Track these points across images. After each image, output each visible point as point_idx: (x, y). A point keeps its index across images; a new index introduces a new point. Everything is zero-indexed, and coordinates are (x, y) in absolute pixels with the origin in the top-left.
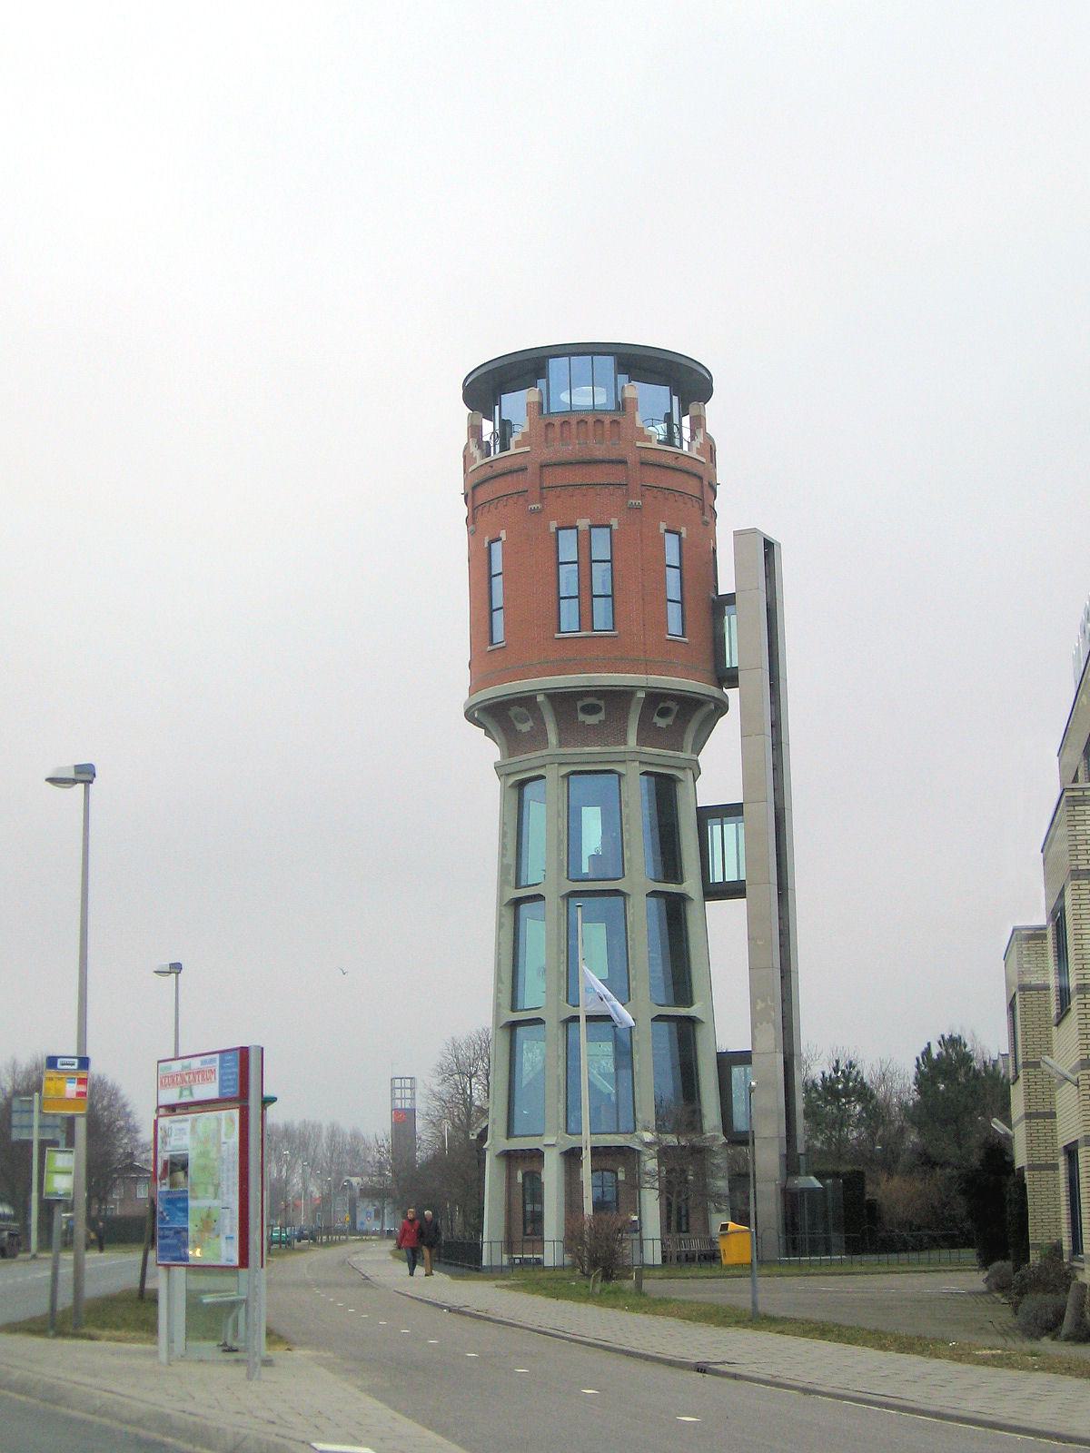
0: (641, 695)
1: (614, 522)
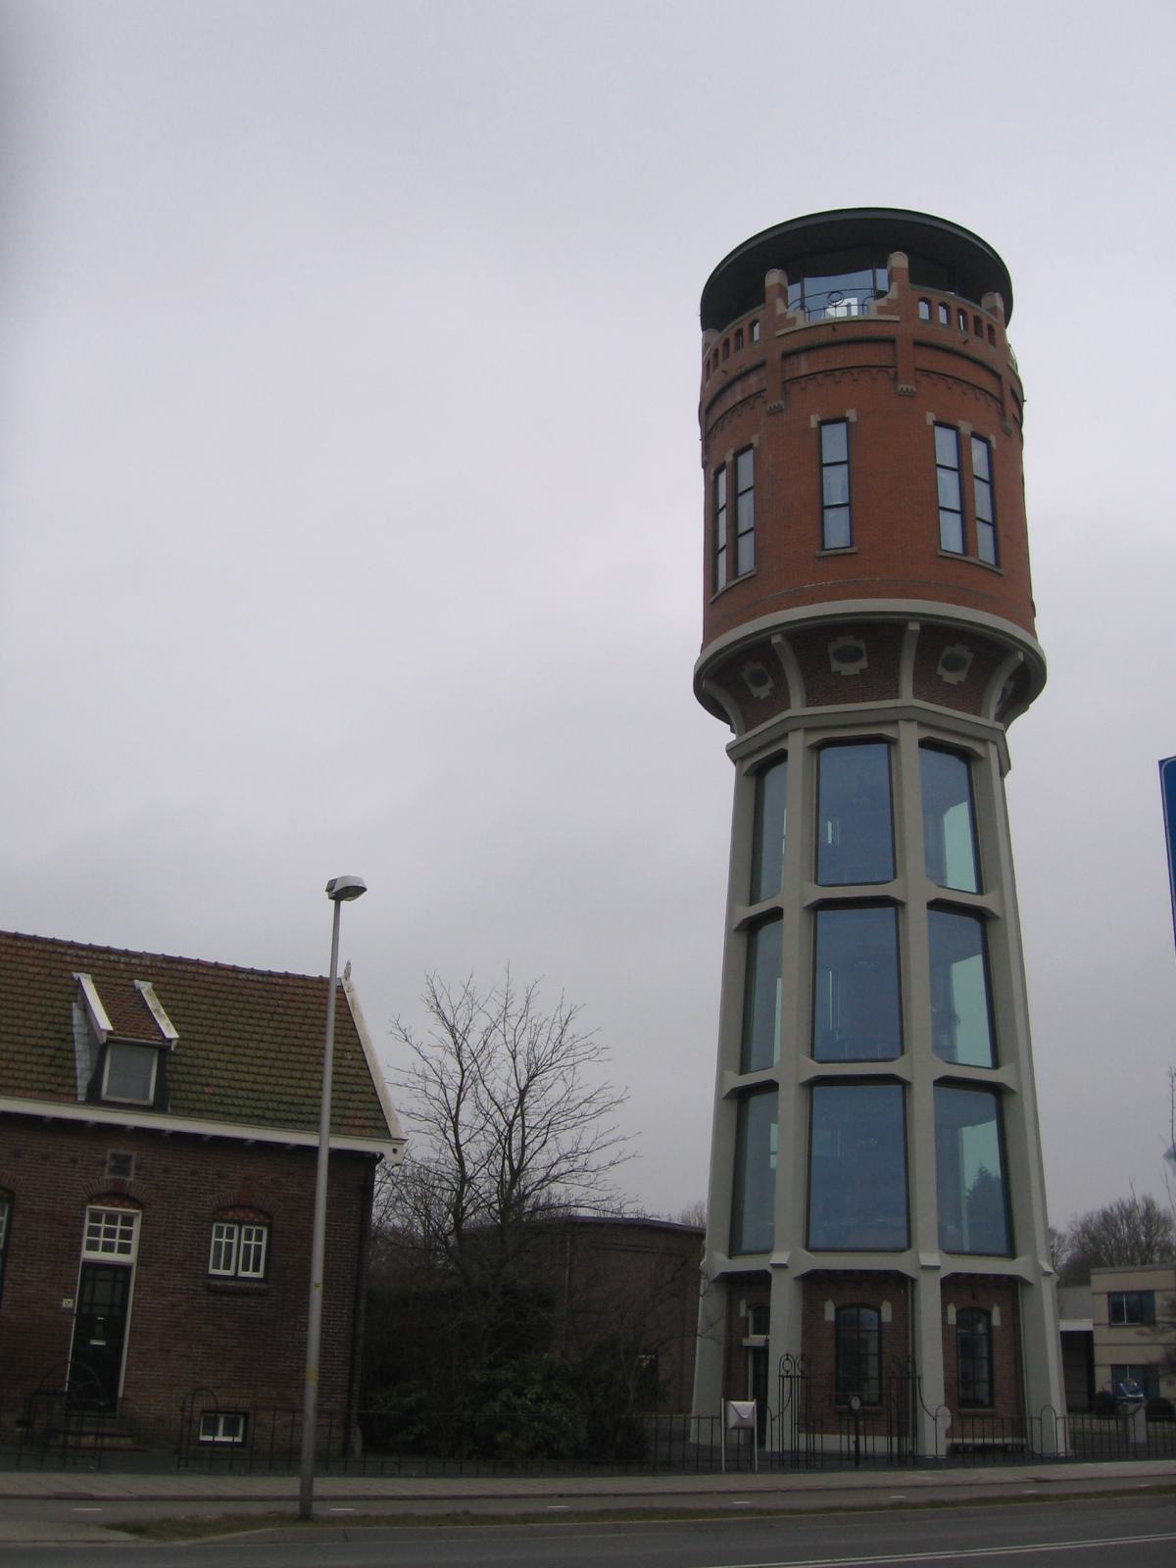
0: (914, 627)
1: (851, 414)
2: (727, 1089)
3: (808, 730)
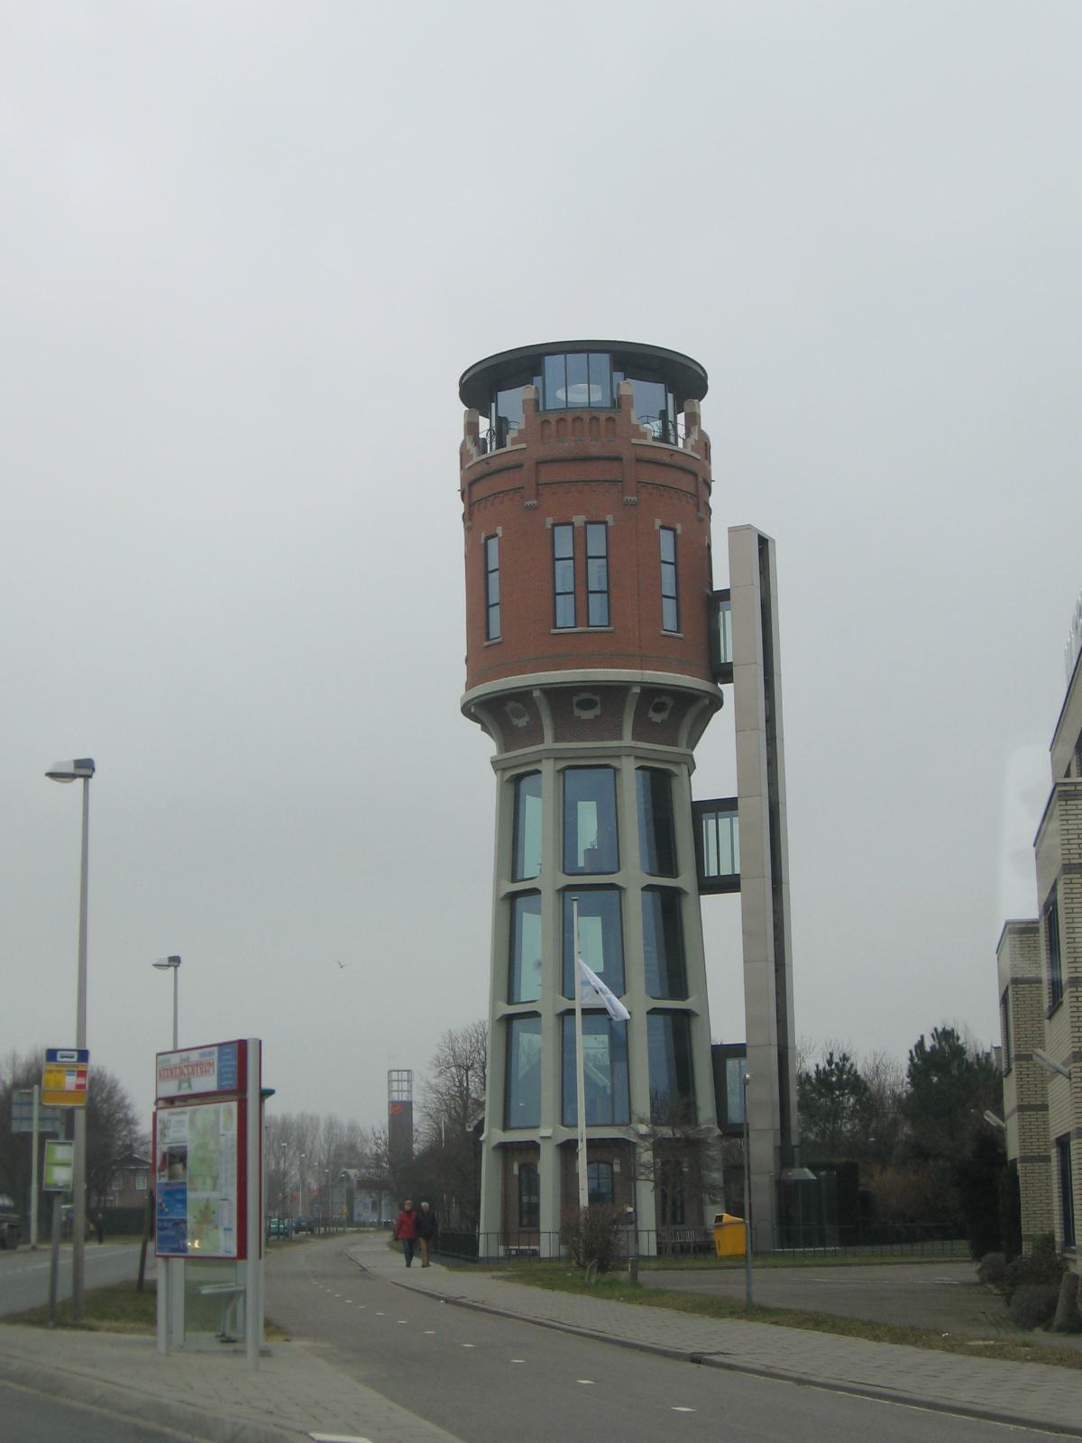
0: (637, 690)
2: (502, 894)
3: (556, 759)
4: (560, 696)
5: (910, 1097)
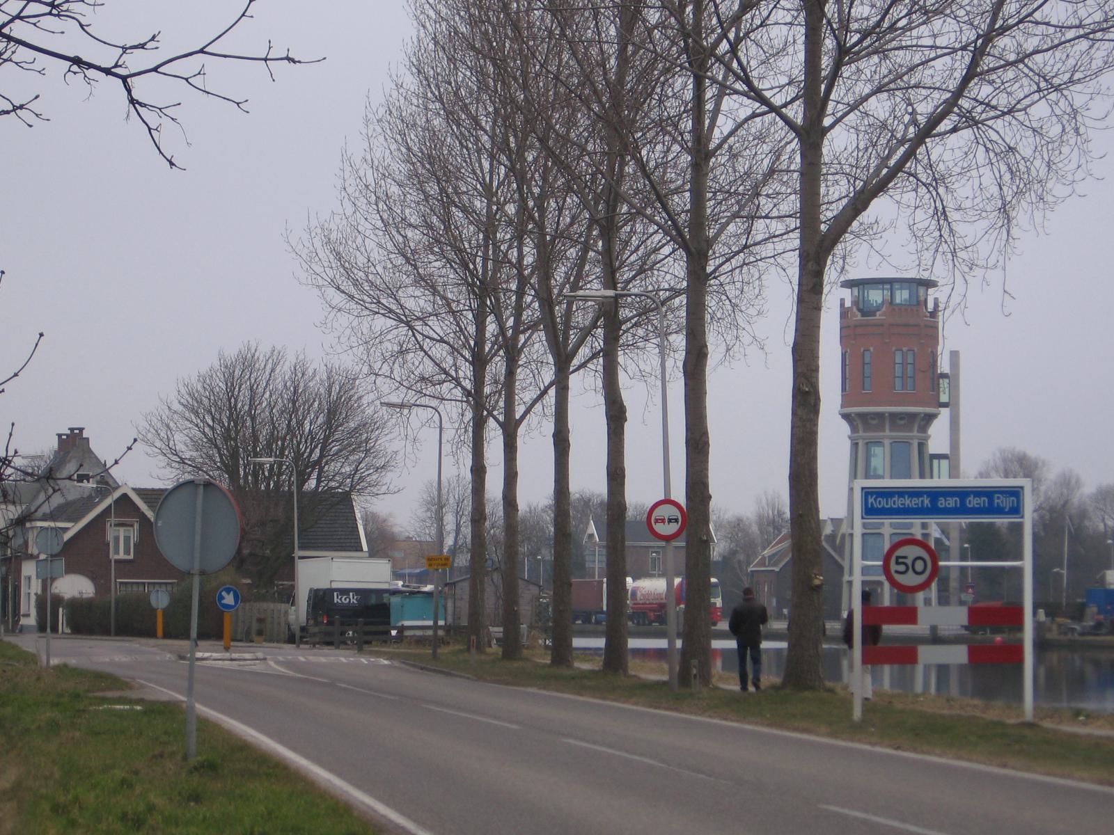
4: (893, 416)
5: (709, 599)
